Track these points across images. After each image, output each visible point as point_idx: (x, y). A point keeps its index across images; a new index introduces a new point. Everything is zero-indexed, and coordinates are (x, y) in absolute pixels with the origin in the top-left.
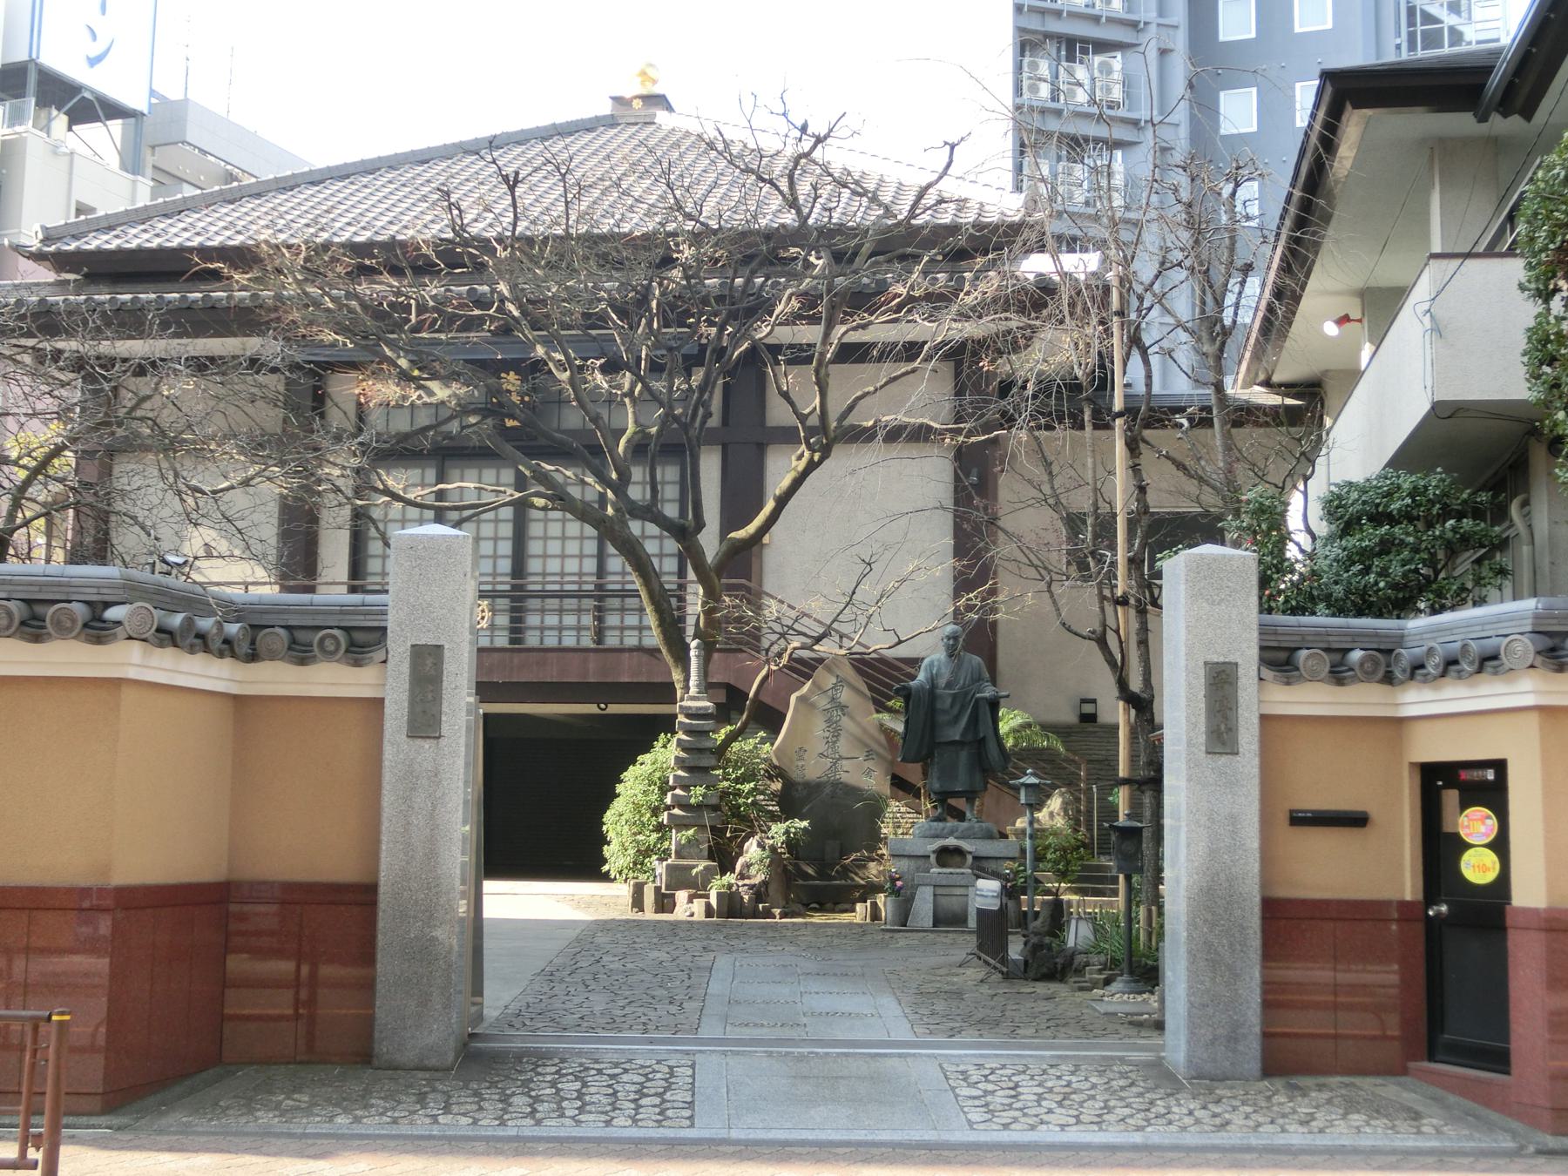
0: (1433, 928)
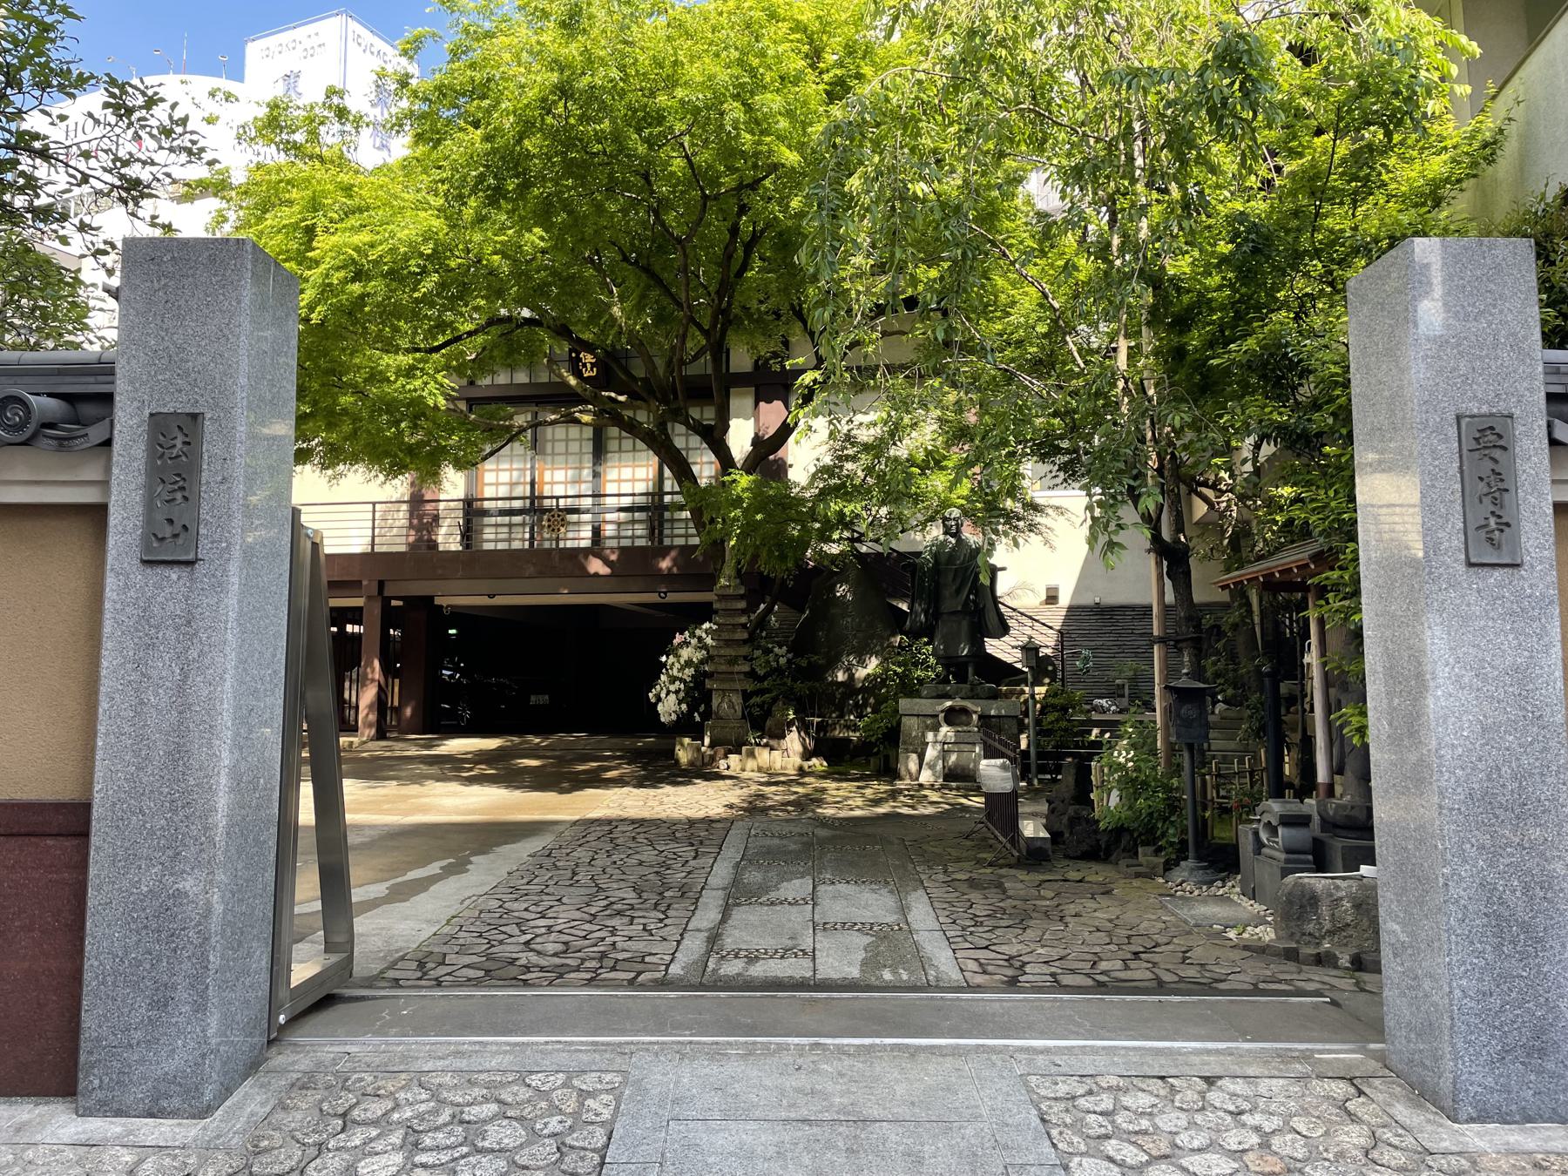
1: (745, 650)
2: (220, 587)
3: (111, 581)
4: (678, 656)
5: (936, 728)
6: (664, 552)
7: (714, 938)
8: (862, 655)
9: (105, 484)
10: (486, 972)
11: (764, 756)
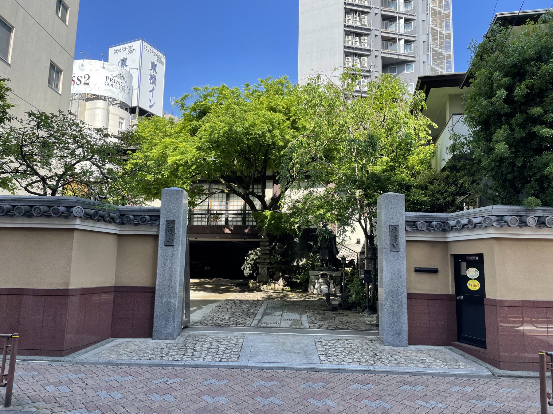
0: (459, 302)
1: (268, 256)
2: (178, 250)
3: (159, 249)
4: (250, 257)
5: (319, 279)
6: (246, 227)
7: (260, 321)
8: (301, 258)
9: (158, 231)
10: (214, 324)
11: (273, 286)
